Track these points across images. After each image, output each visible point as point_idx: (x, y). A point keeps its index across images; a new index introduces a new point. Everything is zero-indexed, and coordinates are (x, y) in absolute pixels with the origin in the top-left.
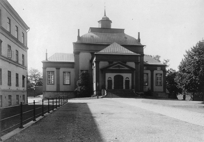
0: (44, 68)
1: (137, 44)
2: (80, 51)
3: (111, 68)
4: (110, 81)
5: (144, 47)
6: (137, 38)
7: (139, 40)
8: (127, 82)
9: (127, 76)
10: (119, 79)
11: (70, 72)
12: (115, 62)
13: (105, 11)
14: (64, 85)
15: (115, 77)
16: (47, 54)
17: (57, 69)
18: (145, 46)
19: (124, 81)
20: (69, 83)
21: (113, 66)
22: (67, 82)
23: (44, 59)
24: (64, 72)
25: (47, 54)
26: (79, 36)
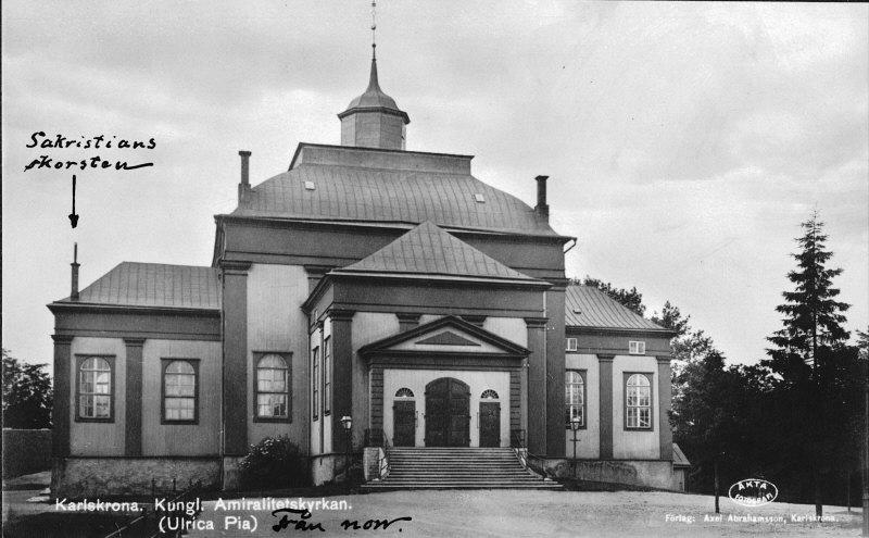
0: (62, 339)
1: (530, 231)
2: (614, 352)
3: (410, 346)
4: (404, 413)
5: (566, 246)
6: (532, 202)
7: (543, 208)
8: (490, 413)
9: (484, 384)
10: (447, 405)
11: (195, 362)
12: (427, 319)
13: (374, 60)
14: (164, 427)
15: (432, 390)
16: (75, 266)
17: (127, 341)
18: (572, 242)
19: (474, 410)
20: (188, 415)
21: (417, 340)
22: (181, 409)
23: (63, 293)
24: (167, 362)
25: (75, 266)
26: (244, 185)
